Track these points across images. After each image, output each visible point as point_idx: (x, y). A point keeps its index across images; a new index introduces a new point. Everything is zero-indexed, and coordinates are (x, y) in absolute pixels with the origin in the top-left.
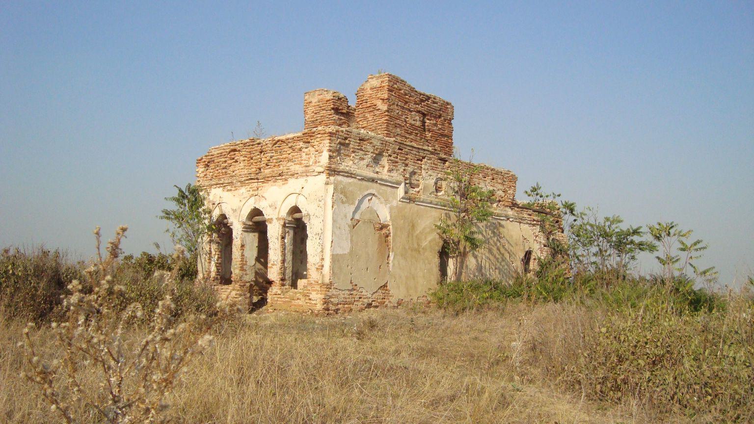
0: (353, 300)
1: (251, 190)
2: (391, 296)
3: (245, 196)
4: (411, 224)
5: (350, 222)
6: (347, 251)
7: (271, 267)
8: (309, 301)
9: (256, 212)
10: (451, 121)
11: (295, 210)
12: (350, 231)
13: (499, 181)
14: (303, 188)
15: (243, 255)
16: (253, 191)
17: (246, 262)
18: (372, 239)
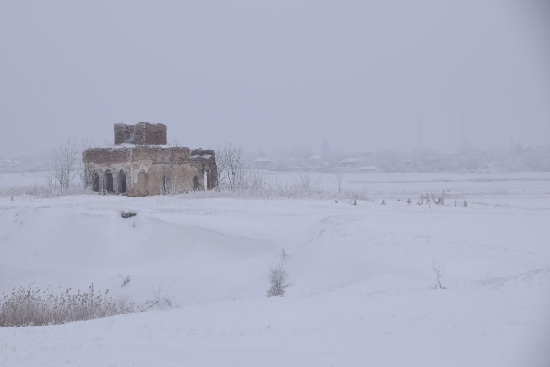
5: (137, 174)
6: (137, 182)
11: (122, 170)
15: (103, 183)
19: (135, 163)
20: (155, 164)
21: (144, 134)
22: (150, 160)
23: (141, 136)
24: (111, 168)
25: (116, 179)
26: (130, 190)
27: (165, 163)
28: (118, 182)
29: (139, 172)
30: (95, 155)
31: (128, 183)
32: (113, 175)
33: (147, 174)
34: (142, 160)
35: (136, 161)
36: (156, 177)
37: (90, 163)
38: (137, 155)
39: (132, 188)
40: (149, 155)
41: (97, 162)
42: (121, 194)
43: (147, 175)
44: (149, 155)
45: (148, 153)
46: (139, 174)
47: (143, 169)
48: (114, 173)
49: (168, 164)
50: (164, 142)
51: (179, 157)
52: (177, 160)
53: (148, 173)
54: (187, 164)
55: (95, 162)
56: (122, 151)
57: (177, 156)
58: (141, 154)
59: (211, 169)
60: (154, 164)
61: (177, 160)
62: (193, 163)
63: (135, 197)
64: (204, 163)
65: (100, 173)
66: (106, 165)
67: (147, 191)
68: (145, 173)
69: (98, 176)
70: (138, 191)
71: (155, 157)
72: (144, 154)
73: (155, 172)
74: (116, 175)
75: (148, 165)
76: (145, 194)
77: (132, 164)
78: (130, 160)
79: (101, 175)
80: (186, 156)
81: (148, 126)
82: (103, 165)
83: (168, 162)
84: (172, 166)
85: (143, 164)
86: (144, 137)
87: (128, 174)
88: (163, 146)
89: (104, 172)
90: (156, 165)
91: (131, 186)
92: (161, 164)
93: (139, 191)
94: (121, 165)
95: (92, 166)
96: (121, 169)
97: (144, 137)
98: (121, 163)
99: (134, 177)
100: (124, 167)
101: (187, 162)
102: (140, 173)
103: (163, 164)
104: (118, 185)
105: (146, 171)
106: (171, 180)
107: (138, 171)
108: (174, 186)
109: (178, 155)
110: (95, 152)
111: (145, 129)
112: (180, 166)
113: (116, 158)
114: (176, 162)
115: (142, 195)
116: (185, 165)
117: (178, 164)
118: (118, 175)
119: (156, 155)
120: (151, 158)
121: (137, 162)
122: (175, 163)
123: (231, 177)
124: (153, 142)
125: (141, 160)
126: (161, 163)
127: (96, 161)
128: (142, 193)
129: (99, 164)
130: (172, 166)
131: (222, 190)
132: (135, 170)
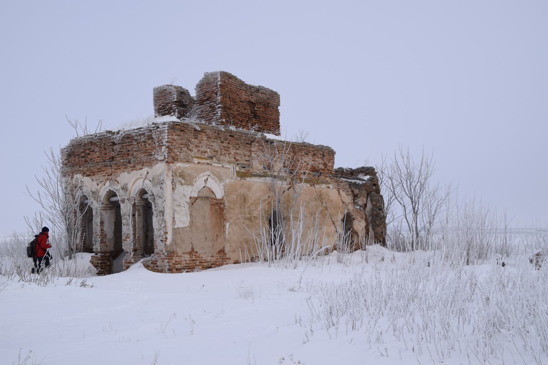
0: (194, 264)
1: (106, 175)
2: (228, 259)
3: (102, 180)
4: (243, 198)
5: (189, 201)
6: (187, 224)
7: (125, 240)
8: (156, 268)
9: (112, 194)
10: (278, 107)
11: (143, 192)
12: (189, 207)
13: (320, 156)
14: (203, 286)
15: (102, 230)
16: (108, 175)
17: (106, 235)
18: (206, 208)
19: (180, 167)
20: (246, 176)
21: (219, 98)
22: (229, 162)
23: (210, 107)
24: (119, 187)
25: (129, 216)
26: (161, 251)
27: (275, 177)
28: (134, 227)
29: (196, 195)
30: (83, 154)
31: (157, 227)
32: (122, 206)
33: (221, 204)
34: (203, 161)
35: (182, 161)
36: (249, 214)
37: (75, 176)
38: (187, 146)
39: (169, 242)
40: (227, 149)
41: (88, 173)
42: (139, 264)
43: (222, 206)
44: (227, 149)
45: (225, 145)
46: (193, 201)
47: (209, 189)
48: (123, 201)
49: (282, 179)
50: (275, 127)
51: (310, 166)
52: (304, 173)
53: (222, 199)
54: (329, 184)
55: (84, 174)
56: (144, 134)
57: (305, 162)
58: (200, 142)
59: (372, 203)
60: (242, 175)
61: (304, 173)
62: (341, 184)
63: (179, 270)
64: (356, 191)
65: (95, 202)
66: (106, 177)
67: (222, 251)
68: (216, 199)
69: (90, 210)
70: (190, 253)
71: (247, 158)
72: (211, 144)
73: (245, 199)
74: (129, 204)
75: (224, 178)
76: (213, 259)
77: (169, 170)
78: (162, 158)
79: (96, 206)
80: (325, 165)
81: (230, 80)
82: (102, 179)
83: (283, 174)
84: (291, 186)
85: (208, 173)
86: (219, 108)
87: (159, 201)
88: (270, 136)
89: (102, 199)
90: (248, 179)
91: (166, 238)
92: (263, 178)
93: (192, 252)
94: (141, 175)
95: (80, 185)
96: (141, 187)
97: (219, 108)
98: (141, 169)
99: (177, 209)
100: (147, 181)
101: (328, 179)
102: (196, 199)
103: (268, 178)
104: (134, 235)
105: (219, 196)
106: (290, 221)
107: (192, 191)
108: (299, 236)
109: (308, 160)
110: (85, 145)
111: (220, 85)
112: (313, 187)
113: (130, 157)
114: (304, 177)
115: (206, 264)
116: (324, 186)
117: (307, 181)
118: (134, 205)
119: (247, 153)
120: (233, 159)
121: (188, 165)
122: (301, 180)
123: (410, 216)
124: (244, 123)
125: (200, 160)
126: (265, 175)
127: (86, 169)
128: (204, 257)
129: (93, 177)
130: (291, 186)
131: (94, 204)
132: (178, 186)
